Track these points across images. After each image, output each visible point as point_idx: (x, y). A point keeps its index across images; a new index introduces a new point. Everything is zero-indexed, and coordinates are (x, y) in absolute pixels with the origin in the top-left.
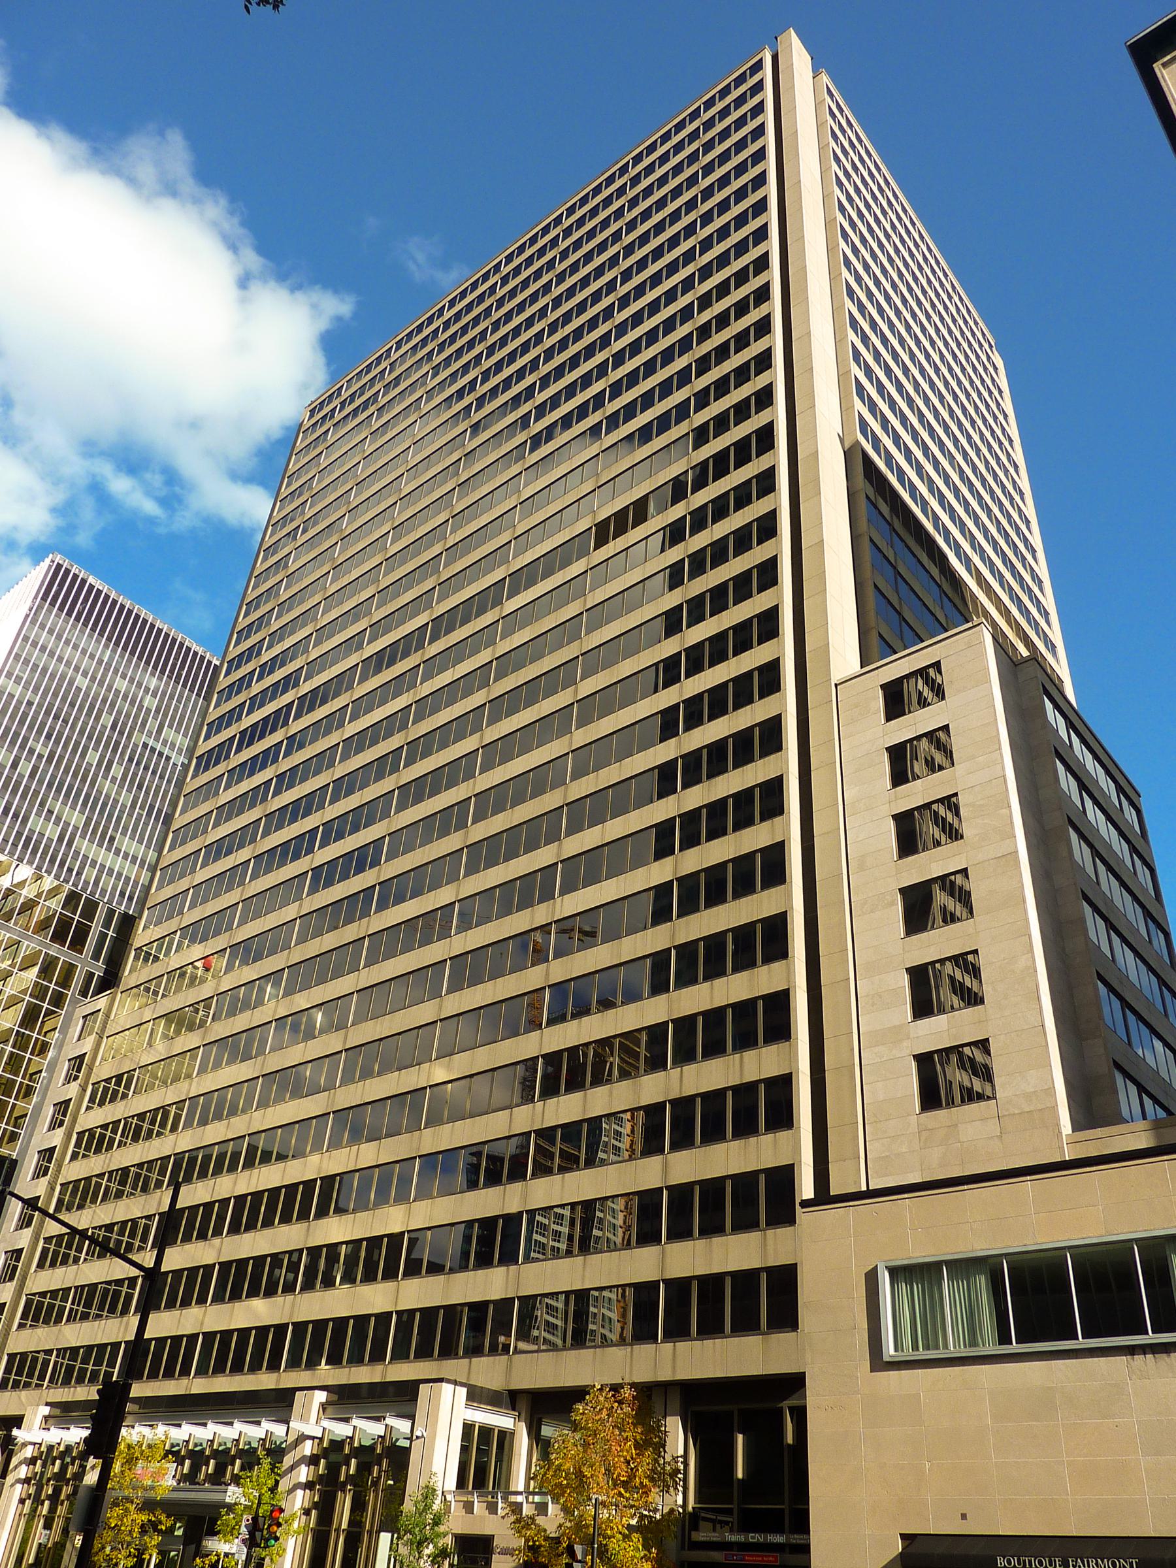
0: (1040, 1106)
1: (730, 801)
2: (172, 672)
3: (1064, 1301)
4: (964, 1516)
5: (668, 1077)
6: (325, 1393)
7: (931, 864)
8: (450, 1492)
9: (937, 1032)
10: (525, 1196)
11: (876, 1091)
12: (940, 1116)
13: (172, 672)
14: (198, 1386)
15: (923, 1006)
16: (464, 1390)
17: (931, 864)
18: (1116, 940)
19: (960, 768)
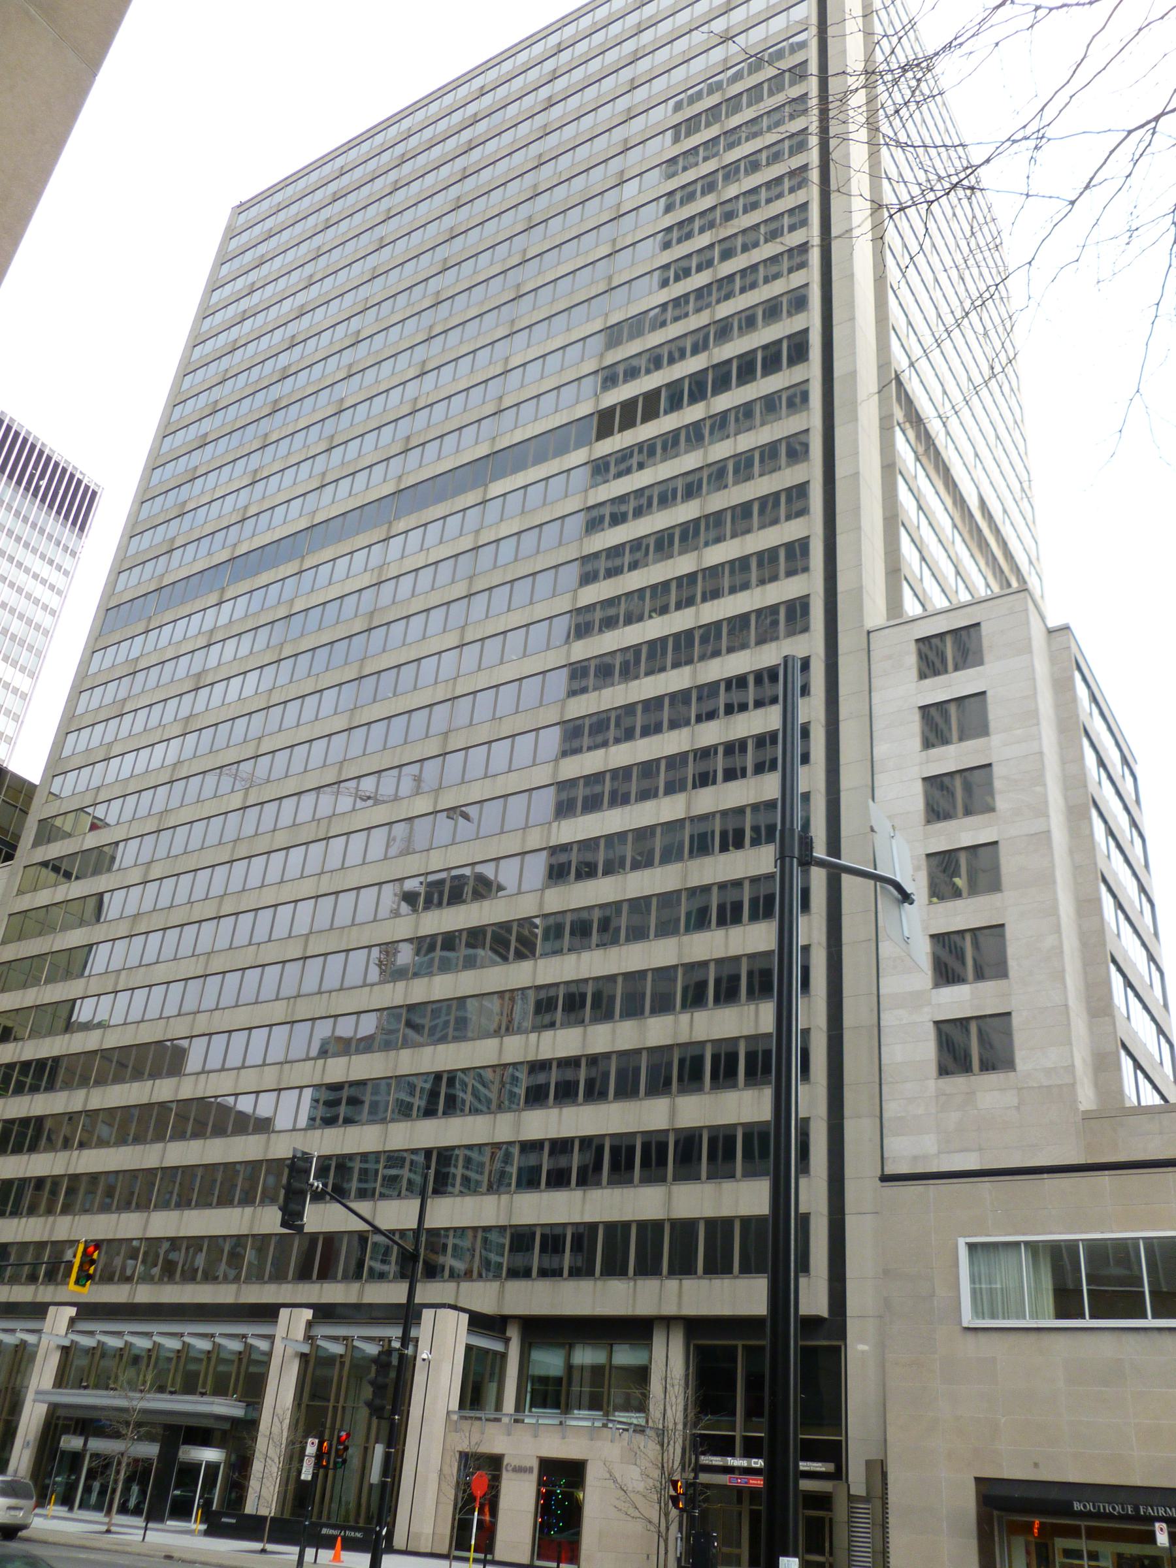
0: (1060, 1082)
1: (671, 640)
2: (29, 483)
3: (1099, 1285)
4: (1036, 1465)
5: (676, 1022)
6: (311, 1311)
7: (963, 833)
8: (454, 1412)
9: (960, 1000)
10: (517, 1125)
11: (895, 1053)
12: (958, 1083)
13: (29, 483)
14: (144, 1294)
15: (947, 971)
16: (466, 1316)
17: (963, 833)
18: (1112, 844)
19: (995, 739)
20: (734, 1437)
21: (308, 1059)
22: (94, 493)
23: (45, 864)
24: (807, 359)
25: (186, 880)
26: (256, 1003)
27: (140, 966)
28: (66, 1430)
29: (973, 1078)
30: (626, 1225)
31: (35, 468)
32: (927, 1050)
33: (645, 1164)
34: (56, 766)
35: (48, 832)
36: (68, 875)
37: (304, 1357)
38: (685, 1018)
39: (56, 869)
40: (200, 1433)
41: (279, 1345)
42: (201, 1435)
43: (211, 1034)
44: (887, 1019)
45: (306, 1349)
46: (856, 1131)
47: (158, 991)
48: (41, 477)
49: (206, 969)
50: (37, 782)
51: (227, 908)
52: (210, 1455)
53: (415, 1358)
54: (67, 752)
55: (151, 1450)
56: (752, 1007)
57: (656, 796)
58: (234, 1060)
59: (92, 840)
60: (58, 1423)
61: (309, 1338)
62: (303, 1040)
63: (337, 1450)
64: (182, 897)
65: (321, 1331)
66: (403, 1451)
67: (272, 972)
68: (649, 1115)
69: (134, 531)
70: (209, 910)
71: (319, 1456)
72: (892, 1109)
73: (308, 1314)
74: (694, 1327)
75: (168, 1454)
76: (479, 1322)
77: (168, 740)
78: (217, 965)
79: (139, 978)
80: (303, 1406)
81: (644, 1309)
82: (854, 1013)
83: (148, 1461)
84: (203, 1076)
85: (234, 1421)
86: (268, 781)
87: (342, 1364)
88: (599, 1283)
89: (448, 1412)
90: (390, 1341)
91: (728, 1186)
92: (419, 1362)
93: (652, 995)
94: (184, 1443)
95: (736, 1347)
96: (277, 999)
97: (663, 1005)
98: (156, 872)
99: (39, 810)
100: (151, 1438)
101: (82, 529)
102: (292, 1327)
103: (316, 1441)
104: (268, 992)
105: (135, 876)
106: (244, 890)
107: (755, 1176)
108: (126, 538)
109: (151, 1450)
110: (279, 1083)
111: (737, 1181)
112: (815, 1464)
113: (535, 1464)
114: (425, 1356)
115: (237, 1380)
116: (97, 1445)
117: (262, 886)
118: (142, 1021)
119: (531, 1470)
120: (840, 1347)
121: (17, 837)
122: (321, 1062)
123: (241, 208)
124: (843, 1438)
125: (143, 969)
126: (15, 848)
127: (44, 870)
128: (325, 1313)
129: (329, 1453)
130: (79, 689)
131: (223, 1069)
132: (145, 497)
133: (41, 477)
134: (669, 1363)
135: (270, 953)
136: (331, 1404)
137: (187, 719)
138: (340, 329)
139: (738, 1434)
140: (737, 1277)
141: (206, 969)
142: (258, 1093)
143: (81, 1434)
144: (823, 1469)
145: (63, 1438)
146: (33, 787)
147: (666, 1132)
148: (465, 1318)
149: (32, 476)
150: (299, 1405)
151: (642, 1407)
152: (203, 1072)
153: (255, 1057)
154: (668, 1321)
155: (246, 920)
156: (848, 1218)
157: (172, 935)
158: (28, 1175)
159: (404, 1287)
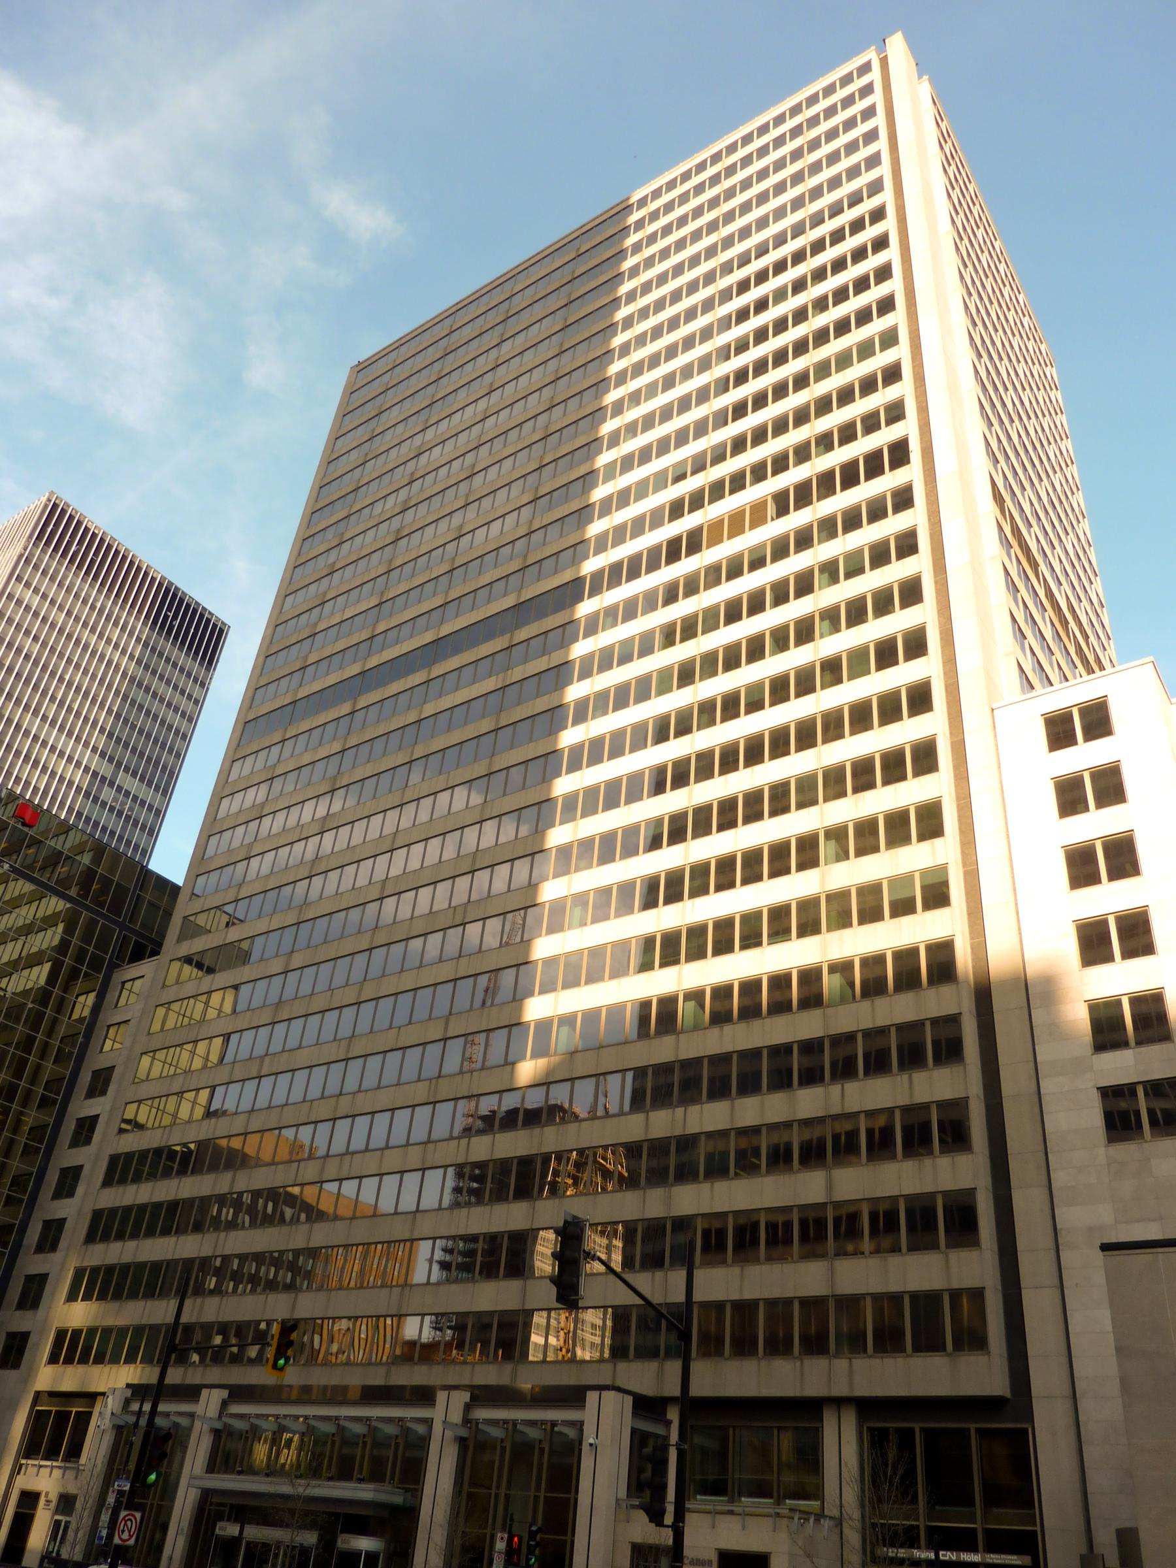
11: (1058, 1121)
12: (1128, 1151)
20: (975, 1530)
21: (451, 1138)
22: (221, 631)
23: (188, 960)
24: (908, 462)
25: (326, 969)
26: (398, 1084)
27: (283, 1051)
28: (220, 1517)
29: (1146, 1145)
30: (788, 1302)
31: (169, 609)
32: (1093, 1116)
33: (804, 1238)
34: (200, 865)
35: (190, 930)
36: (210, 971)
37: (462, 1442)
38: (835, 1089)
39: (200, 966)
40: (359, 1520)
41: (437, 1428)
42: (360, 1526)
43: (354, 1116)
44: (1047, 1086)
45: (464, 1433)
46: (1026, 1201)
47: (301, 1076)
48: (175, 617)
49: (348, 1051)
50: (179, 880)
51: (368, 993)
52: (365, 1544)
53: (580, 1443)
54: (210, 852)
55: (310, 1538)
56: (905, 1077)
57: (554, 990)
58: (378, 1140)
59: (233, 934)
60: (210, 1508)
61: (466, 1421)
62: (446, 1119)
63: (529, 1546)
64: (322, 986)
65: (482, 1414)
66: (573, 1542)
67: (414, 1055)
68: (806, 1188)
69: (267, 654)
70: (350, 996)
71: (510, 1552)
72: (1060, 1179)
73: (466, 1396)
74: (867, 1407)
75: (327, 1543)
76: (646, 1406)
77: (307, 838)
78: (358, 1049)
79: (283, 1063)
80: (464, 1494)
81: (813, 1388)
82: (1012, 1081)
83: (305, 1551)
84: (348, 1158)
85: (394, 1509)
86: (147, 1080)
87: (503, 1449)
88: (763, 1363)
89: (617, 1500)
90: (477, 1424)
91: (894, 1260)
92: (585, 1448)
93: (800, 1070)
94: (343, 1532)
95: (912, 1430)
96: (419, 1080)
97: (811, 1077)
98: (297, 961)
99: (182, 908)
100: (311, 1526)
101: (210, 662)
102: (448, 1410)
103: (506, 1536)
104: (410, 1073)
105: (276, 966)
106: (383, 976)
107: (918, 1249)
108: (262, 659)
109: (310, 1538)
110: (423, 1161)
111: (902, 1255)
112: (1010, 1557)
113: (714, 1557)
114: (591, 1441)
115: (331, 1459)
116: (253, 1532)
117: (402, 971)
118: (286, 1104)
119: (710, 1563)
120: (1025, 1431)
121: (162, 936)
122: (464, 1141)
123: (361, 368)
124: (1038, 1529)
125: (286, 1055)
126: (160, 945)
127: (186, 966)
128: (239, 1393)
129: (519, 1549)
130: (218, 798)
131: (367, 1150)
132: (277, 623)
133: (175, 617)
134: (842, 1447)
135: (411, 1035)
136: (542, 1494)
137: (324, 819)
138: (456, 465)
139: (922, 1524)
140: (911, 1356)
141: (348, 1051)
142: (402, 1172)
143: (236, 1521)
144: (1019, 1563)
145: (219, 1524)
146: (175, 889)
147: (823, 1205)
148: (629, 1400)
149: (166, 617)
150: (460, 1492)
151: (817, 1493)
152: (347, 1153)
153: (398, 1137)
154: (839, 1402)
155: (386, 1005)
156: (1024, 1292)
157: (314, 1021)
158: (177, 1257)
159: (674, 1368)
